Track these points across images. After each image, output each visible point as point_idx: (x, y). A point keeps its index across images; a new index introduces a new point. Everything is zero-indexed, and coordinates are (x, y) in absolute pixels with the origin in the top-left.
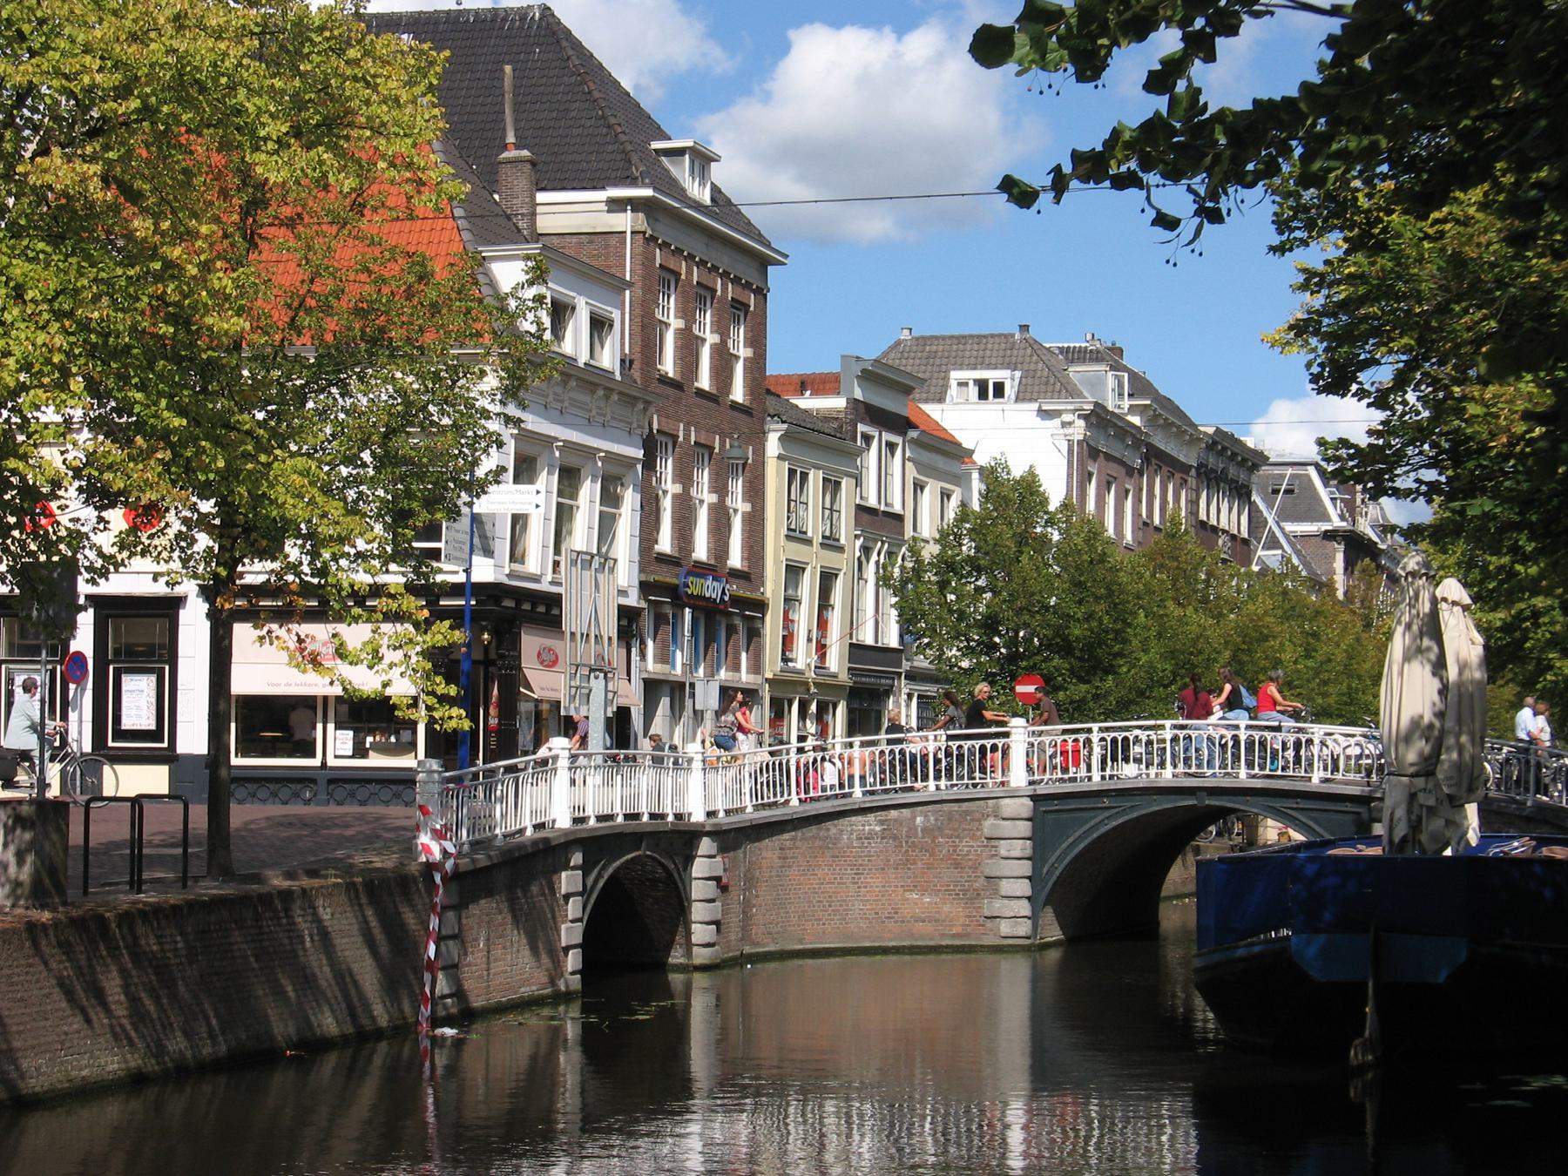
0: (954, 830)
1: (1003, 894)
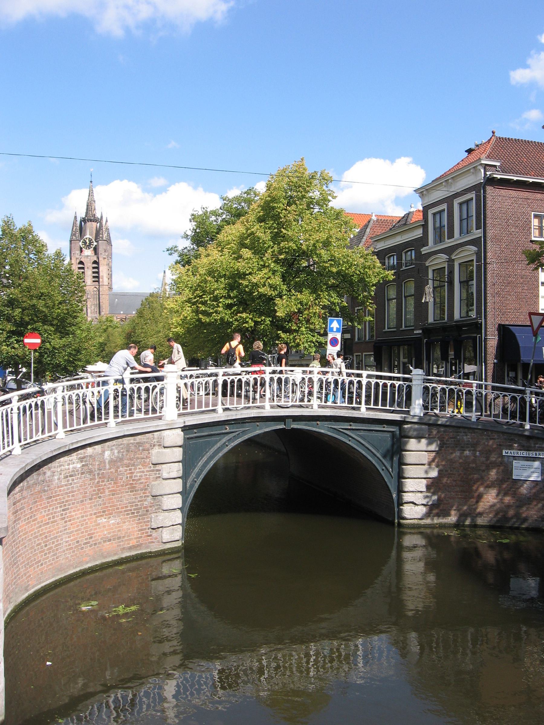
0: (131, 459)
1: (165, 508)
